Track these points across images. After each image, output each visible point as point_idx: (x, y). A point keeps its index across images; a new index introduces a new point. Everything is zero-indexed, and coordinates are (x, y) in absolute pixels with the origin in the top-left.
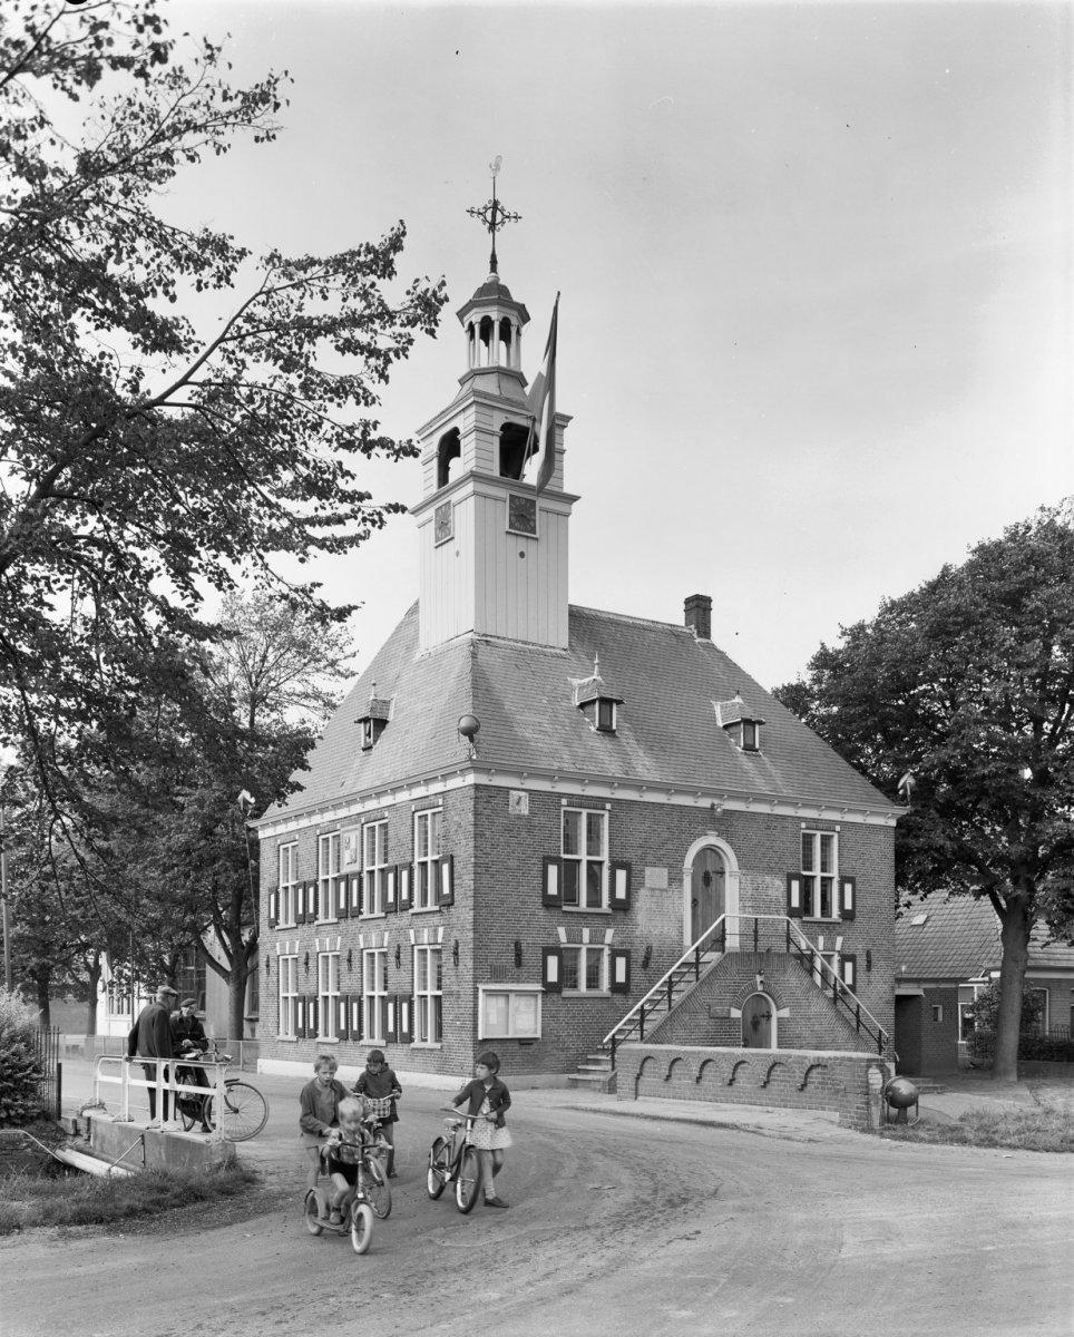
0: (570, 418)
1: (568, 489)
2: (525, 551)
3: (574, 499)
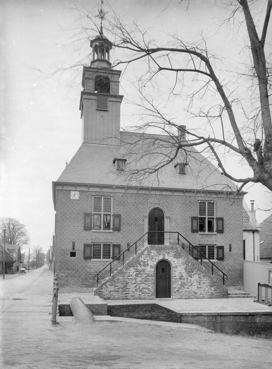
1: (120, 94)
2: (101, 118)
3: (122, 97)
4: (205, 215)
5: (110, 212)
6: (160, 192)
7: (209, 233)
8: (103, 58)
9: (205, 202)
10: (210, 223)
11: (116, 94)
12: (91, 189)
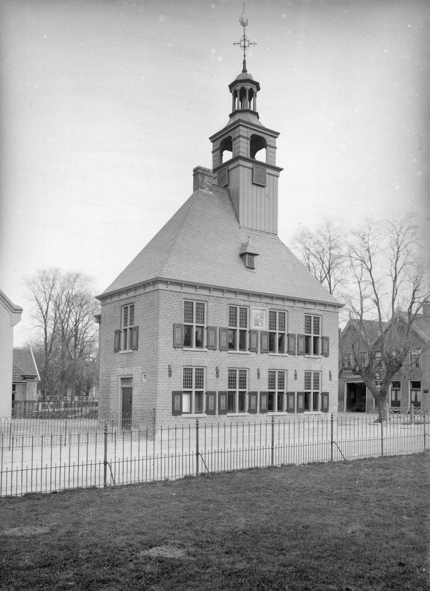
0: (278, 134)
1: (278, 165)
3: (280, 170)
4: (236, 326)
5: (203, 323)
6: (247, 297)
7: (197, 349)
8: (241, 108)
9: (285, 313)
10: (281, 340)
11: (272, 164)
12: (227, 295)
